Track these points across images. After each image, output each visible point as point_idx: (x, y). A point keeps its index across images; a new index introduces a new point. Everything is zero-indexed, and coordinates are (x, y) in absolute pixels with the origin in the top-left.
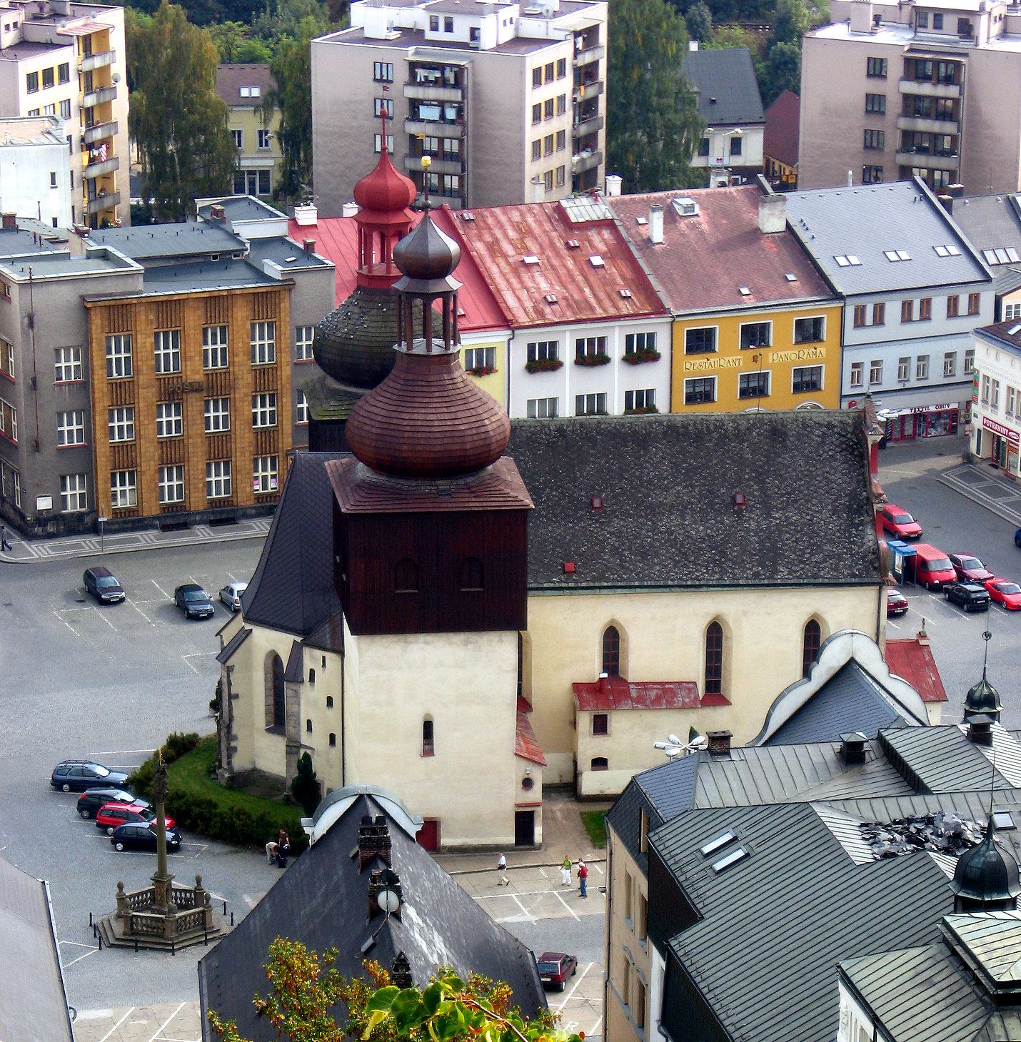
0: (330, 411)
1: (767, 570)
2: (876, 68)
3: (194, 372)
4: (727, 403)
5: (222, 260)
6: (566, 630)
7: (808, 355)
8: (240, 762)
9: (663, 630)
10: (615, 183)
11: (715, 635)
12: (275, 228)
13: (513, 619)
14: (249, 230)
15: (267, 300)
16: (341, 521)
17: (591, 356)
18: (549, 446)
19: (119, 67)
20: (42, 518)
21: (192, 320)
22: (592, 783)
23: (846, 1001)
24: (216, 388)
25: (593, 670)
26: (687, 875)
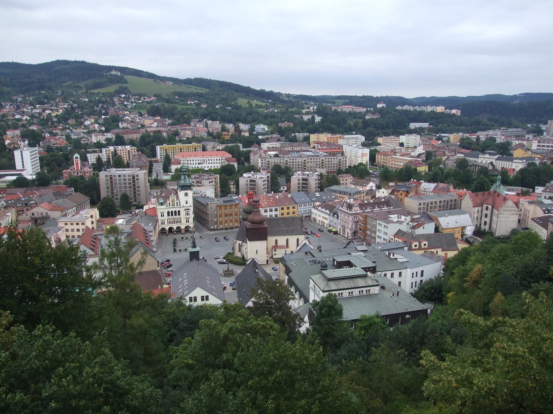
0: (244, 217)
1: (292, 233)
2: (299, 180)
3: (228, 213)
4: (285, 215)
5: (232, 201)
6: (271, 240)
7: (294, 210)
8: (236, 255)
9: (282, 240)
10: (273, 192)
11: (287, 240)
12: (237, 197)
13: (266, 239)
14: (234, 198)
15: (236, 205)
16: (247, 228)
17: (271, 211)
18: (271, 220)
19: (219, 181)
20: (212, 229)
21: (228, 207)
22: (274, 257)
23: (311, 281)
24: (231, 215)
25: (274, 244)
26: (290, 267)
